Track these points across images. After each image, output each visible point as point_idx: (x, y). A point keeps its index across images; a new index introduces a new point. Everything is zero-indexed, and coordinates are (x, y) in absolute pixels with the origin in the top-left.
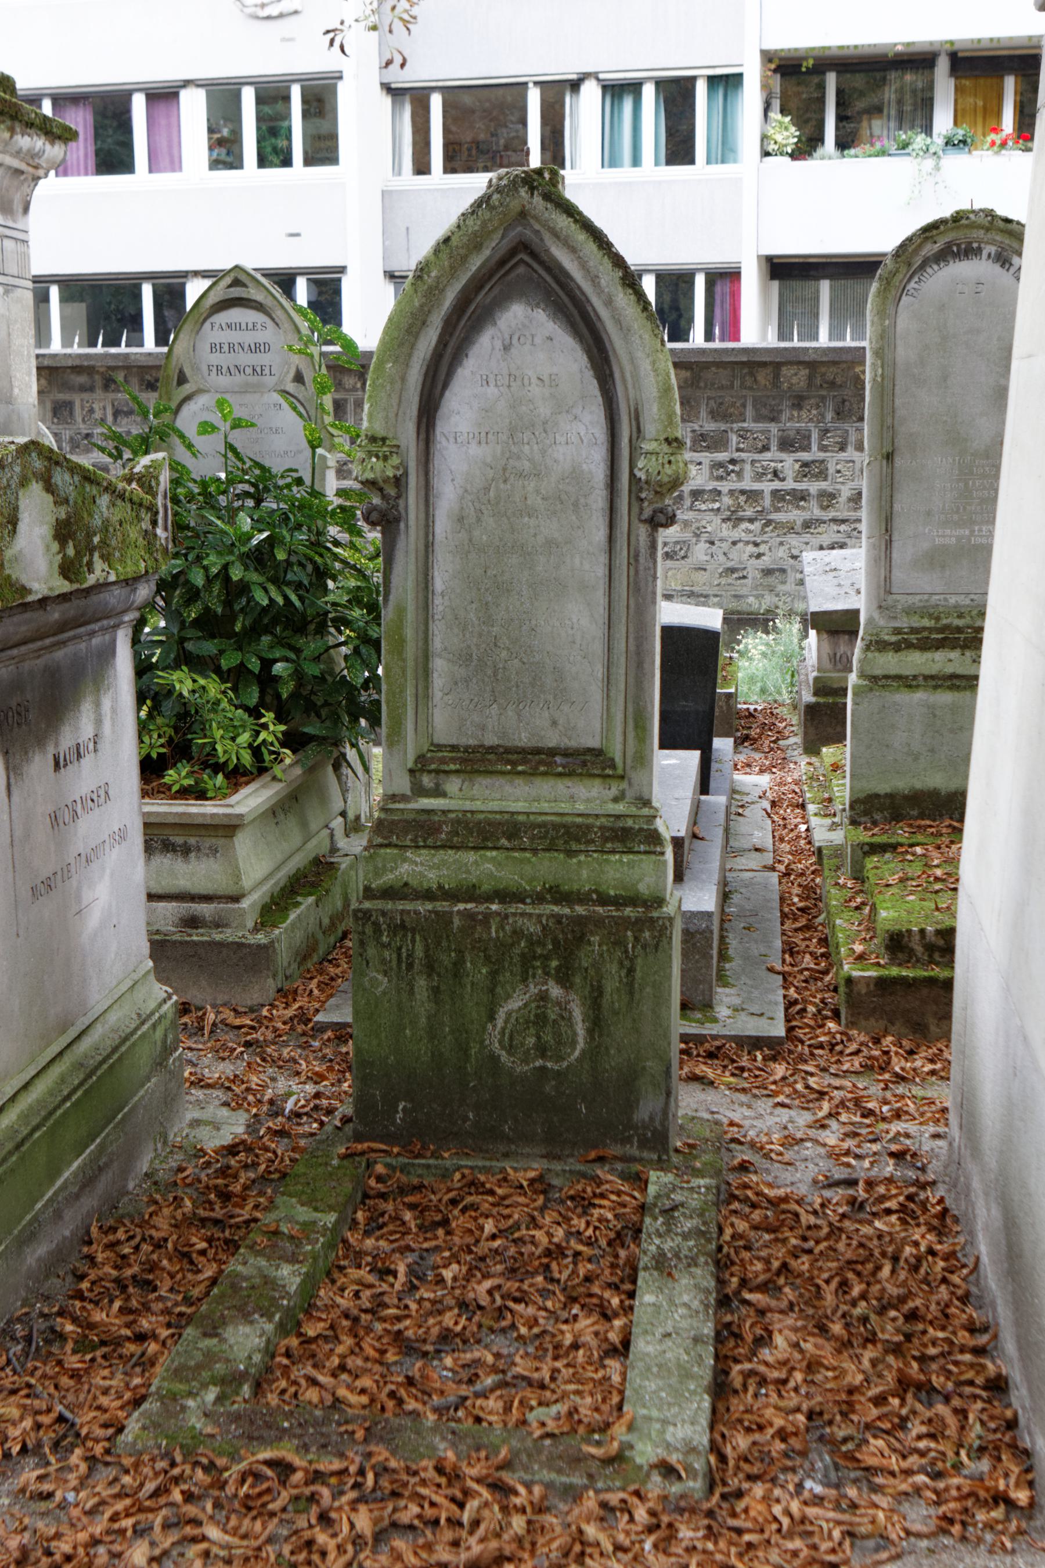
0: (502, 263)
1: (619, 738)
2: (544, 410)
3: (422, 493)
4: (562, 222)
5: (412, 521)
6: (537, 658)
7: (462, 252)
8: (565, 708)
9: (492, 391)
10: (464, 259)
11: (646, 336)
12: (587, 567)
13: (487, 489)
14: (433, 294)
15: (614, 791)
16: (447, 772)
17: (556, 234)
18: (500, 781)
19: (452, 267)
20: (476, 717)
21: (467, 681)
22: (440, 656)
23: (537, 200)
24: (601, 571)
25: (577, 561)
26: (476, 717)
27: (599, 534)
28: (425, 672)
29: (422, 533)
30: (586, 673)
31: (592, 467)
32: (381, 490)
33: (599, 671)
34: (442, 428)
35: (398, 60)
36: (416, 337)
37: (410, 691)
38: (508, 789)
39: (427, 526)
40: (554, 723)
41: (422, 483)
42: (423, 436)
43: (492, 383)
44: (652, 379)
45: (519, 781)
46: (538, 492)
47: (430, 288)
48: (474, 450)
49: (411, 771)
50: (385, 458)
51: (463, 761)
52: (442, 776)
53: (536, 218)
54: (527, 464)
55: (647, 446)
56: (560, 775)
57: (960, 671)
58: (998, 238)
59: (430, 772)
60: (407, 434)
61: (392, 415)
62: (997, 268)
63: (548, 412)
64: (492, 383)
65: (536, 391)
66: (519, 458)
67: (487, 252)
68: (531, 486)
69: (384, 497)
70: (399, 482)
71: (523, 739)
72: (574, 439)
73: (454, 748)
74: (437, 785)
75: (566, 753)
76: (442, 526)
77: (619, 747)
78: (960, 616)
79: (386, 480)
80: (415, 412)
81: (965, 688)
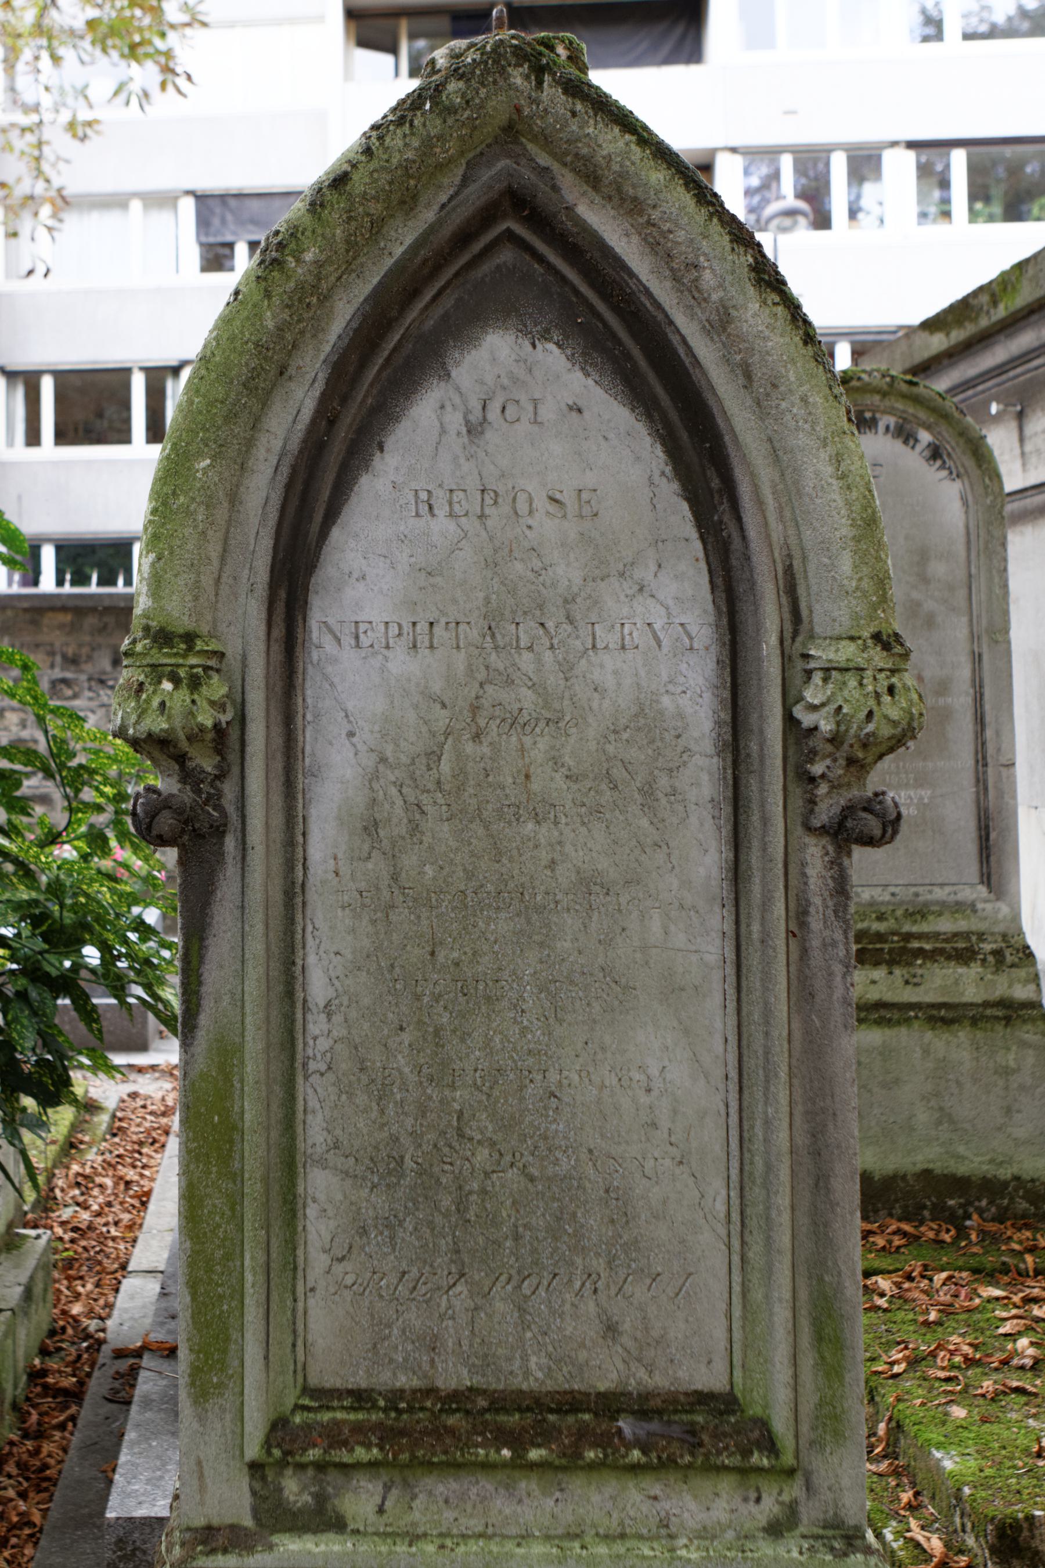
0: (463, 238)
1: (782, 1374)
2: (568, 572)
3: (279, 765)
4: (612, 142)
5: (256, 835)
6: (565, 1165)
7: (376, 208)
8: (638, 1291)
9: (441, 526)
10: (377, 227)
11: (817, 399)
12: (680, 939)
13: (434, 756)
14: (308, 301)
15: (769, 1507)
16: (344, 1467)
17: (591, 176)
18: (486, 1484)
19: (350, 244)
20: (413, 1317)
21: (390, 1225)
22: (323, 1163)
23: (551, 93)
24: (713, 949)
25: (655, 925)
26: (413, 1317)
27: (706, 859)
28: (288, 1206)
29: (277, 862)
30: (685, 1198)
31: (684, 701)
32: (181, 759)
33: (718, 1197)
34: (323, 613)
35: (41, 270)
36: (265, 404)
37: (251, 1259)
38: (502, 1506)
39: (290, 843)
40: (611, 1330)
41: (278, 741)
42: (279, 632)
43: (441, 511)
44: (835, 495)
45: (527, 1484)
46: (556, 762)
47: (301, 287)
48: (401, 663)
49: (255, 1468)
50: (195, 683)
51: (387, 1435)
52: (333, 1476)
53: (546, 140)
54: (528, 698)
55: (822, 653)
56: (635, 1469)
57: (889, 997)
58: (899, 405)
59: (301, 1467)
60: (243, 627)
61: (207, 581)
62: (898, 445)
63: (577, 577)
64: (441, 511)
65: (546, 526)
66: (510, 682)
67: (428, 216)
68: (540, 747)
69: (188, 775)
70: (228, 740)
71: (534, 1372)
72: (639, 637)
73: (361, 1398)
74: (321, 1499)
75: (645, 1406)
76: (325, 841)
77: (782, 1395)
78: (881, 918)
79: (195, 736)
80: (262, 576)
81: (899, 1023)
